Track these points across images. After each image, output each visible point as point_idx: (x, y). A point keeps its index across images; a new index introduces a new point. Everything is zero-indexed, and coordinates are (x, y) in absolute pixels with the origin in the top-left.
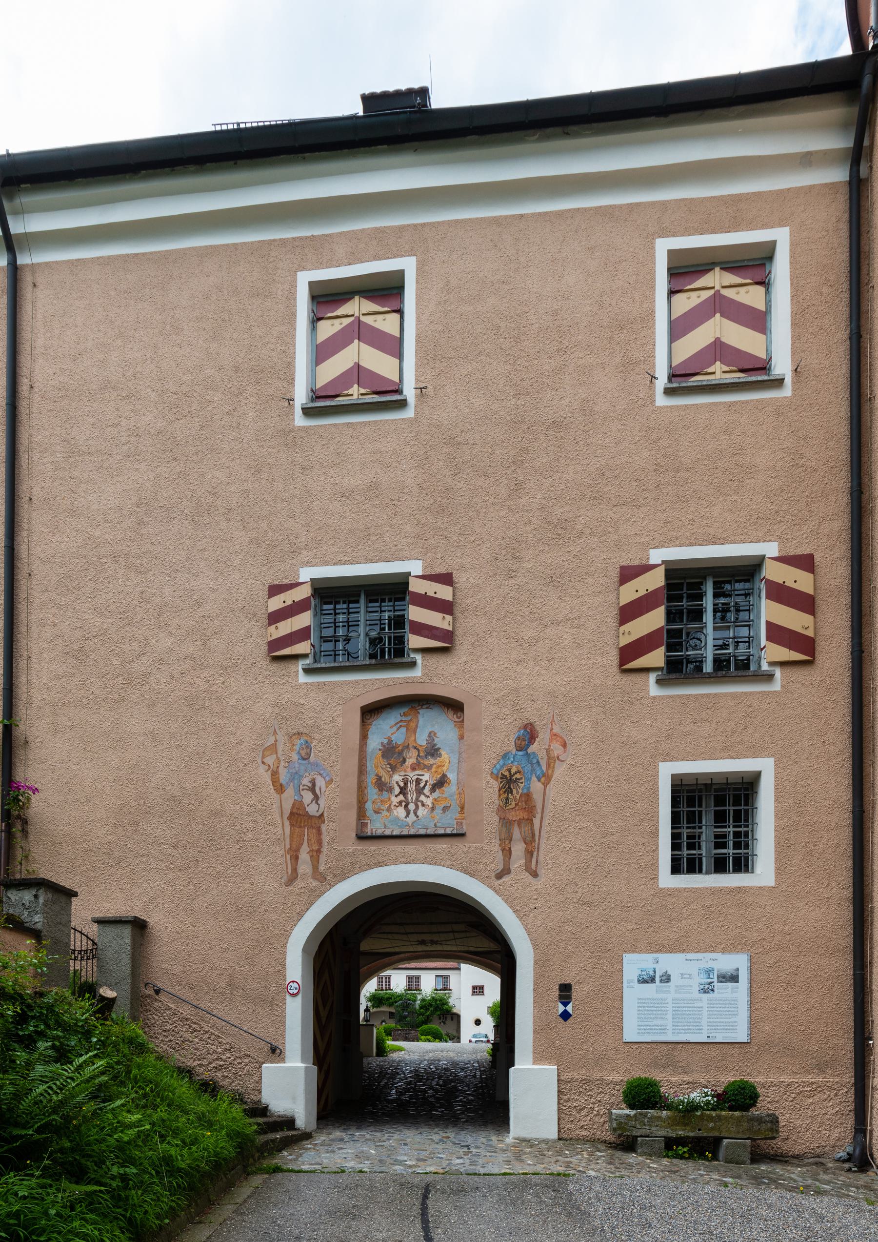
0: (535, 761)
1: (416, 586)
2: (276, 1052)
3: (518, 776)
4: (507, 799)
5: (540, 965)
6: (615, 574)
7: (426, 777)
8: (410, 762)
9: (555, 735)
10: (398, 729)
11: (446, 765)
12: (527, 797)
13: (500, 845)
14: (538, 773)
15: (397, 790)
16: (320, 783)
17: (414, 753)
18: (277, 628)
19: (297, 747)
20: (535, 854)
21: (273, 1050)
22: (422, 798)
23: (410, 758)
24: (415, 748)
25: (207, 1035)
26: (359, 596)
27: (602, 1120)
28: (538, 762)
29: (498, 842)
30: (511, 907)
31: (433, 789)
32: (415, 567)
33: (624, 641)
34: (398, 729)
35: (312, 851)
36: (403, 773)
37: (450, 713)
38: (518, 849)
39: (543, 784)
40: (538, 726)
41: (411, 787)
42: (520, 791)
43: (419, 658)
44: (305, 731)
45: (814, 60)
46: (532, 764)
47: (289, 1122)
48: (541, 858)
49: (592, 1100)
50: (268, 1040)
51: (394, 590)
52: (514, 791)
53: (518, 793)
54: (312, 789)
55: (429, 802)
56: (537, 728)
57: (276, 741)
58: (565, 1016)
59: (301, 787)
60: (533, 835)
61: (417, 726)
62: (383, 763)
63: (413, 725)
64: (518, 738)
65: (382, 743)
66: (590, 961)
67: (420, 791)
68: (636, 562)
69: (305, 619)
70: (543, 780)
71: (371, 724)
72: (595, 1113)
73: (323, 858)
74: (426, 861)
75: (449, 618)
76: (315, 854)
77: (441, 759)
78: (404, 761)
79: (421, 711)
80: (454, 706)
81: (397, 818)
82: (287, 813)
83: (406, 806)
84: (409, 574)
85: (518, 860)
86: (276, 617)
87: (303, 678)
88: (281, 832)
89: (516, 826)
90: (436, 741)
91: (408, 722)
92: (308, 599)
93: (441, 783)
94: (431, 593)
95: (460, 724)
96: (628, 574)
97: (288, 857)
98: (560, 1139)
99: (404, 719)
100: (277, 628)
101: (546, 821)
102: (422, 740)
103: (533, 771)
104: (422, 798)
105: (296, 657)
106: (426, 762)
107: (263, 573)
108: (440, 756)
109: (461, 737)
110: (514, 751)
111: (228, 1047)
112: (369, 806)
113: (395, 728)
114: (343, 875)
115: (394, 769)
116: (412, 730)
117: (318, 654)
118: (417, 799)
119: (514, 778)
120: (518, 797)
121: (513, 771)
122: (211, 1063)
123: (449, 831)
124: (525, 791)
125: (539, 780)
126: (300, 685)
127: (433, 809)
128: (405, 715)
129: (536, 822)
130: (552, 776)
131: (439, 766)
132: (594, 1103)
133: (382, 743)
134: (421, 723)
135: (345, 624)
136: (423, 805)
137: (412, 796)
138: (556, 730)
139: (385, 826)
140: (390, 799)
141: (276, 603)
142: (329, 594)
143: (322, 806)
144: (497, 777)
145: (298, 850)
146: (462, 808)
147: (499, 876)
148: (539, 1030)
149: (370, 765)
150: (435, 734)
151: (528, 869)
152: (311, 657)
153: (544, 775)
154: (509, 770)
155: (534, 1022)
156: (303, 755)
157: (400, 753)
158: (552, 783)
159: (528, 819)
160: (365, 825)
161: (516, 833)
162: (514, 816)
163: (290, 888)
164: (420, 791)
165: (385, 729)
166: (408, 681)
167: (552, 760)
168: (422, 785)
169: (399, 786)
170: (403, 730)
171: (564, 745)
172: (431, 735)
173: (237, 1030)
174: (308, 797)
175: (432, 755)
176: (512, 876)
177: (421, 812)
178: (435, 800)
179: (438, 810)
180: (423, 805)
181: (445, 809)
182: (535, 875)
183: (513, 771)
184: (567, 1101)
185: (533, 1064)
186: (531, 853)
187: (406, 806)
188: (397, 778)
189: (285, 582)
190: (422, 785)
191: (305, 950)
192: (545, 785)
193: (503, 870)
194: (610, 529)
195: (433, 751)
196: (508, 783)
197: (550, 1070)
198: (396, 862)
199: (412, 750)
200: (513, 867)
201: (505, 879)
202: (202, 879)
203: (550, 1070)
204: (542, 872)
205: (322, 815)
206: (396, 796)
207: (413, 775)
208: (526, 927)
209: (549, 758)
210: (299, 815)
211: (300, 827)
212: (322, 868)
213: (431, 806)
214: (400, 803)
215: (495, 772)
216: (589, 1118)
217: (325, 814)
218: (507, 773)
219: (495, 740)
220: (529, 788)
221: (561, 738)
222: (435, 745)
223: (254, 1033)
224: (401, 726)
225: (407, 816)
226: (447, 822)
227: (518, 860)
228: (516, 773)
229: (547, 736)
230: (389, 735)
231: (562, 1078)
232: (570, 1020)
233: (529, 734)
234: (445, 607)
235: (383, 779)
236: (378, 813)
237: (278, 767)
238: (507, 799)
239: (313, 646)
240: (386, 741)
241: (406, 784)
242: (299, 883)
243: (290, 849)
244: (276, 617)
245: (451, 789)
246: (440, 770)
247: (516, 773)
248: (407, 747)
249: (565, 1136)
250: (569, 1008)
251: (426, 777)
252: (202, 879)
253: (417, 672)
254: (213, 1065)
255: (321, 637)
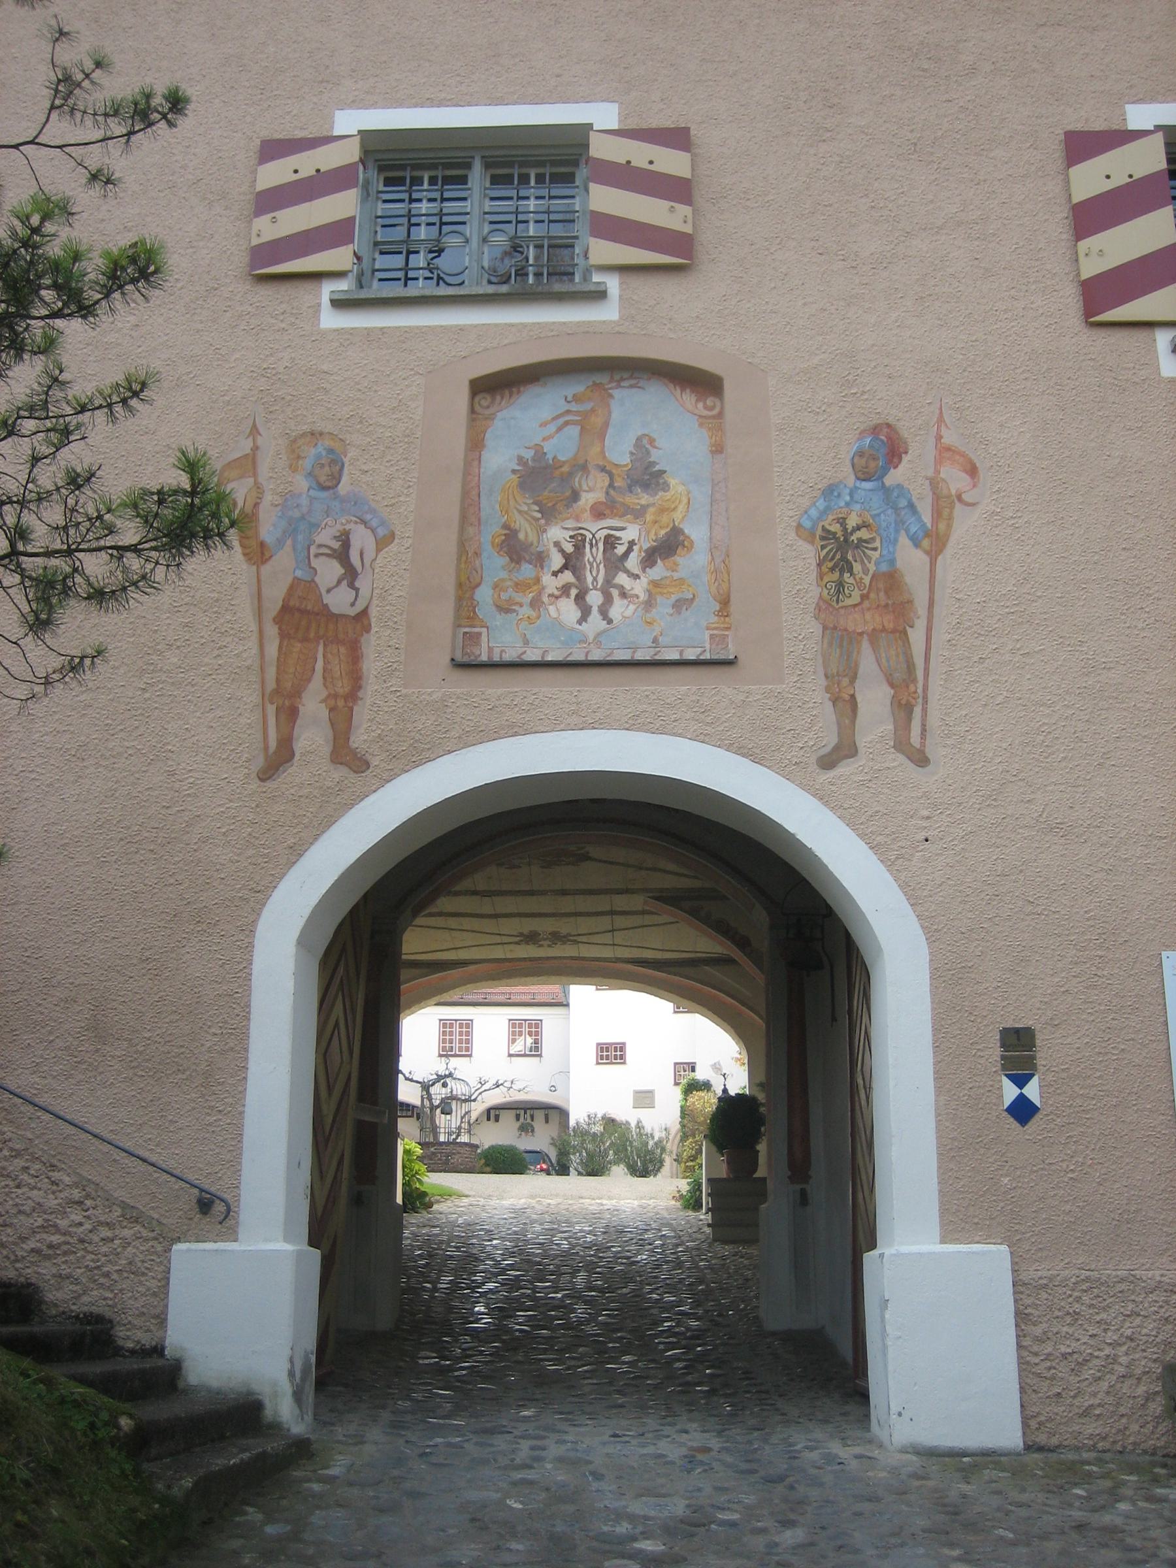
0: (903, 503)
1: (600, 148)
2: (212, 1209)
3: (864, 534)
4: (840, 585)
5: (949, 981)
6: (1055, 149)
7: (631, 532)
8: (588, 499)
9: (948, 449)
10: (560, 429)
11: (682, 508)
12: (891, 580)
13: (828, 689)
14: (913, 529)
15: (557, 561)
16: (362, 539)
17: (602, 481)
18: (274, 220)
19: (307, 464)
20: (918, 710)
21: (205, 1205)
22: (622, 579)
23: (591, 490)
24: (603, 469)
25: (20, 1163)
26: (468, 166)
27: (1141, 1390)
28: (911, 506)
29: (822, 682)
30: (862, 836)
31: (649, 560)
32: (602, 116)
33: (1091, 268)
34: (560, 429)
35: (335, 696)
36: (570, 524)
37: (689, 398)
38: (874, 698)
39: (927, 553)
40: (905, 430)
41: (593, 555)
42: (872, 568)
43: (613, 283)
44: (328, 427)
45: (792, 831)
46: (896, 510)
47: (243, 1414)
48: (934, 720)
49: (1111, 1337)
50: (191, 1177)
51: (552, 160)
52: (857, 567)
53: (866, 571)
54: (342, 554)
55: (639, 588)
56: (905, 434)
57: (255, 448)
58: (1023, 1111)
59: (313, 550)
60: (910, 667)
61: (606, 424)
62: (525, 503)
63: (596, 421)
64: (860, 453)
65: (520, 459)
66: (1077, 970)
67: (615, 564)
68: (1098, 126)
69: (343, 205)
70: (926, 543)
71: (491, 418)
72: (1121, 1370)
73: (363, 713)
74: (634, 724)
75: (684, 210)
76: (341, 703)
77: (668, 495)
78: (575, 496)
79: (616, 393)
80: (699, 382)
81: (558, 623)
82: (273, 605)
83: (580, 599)
84: (590, 126)
85: (312, 737)
86: (272, 200)
87: (331, 320)
88: (255, 650)
89: (865, 645)
90: (655, 455)
91: (586, 415)
92: (351, 167)
93: (669, 546)
94: (640, 162)
95: (715, 423)
96: (1082, 146)
97: (271, 710)
98: (1028, 1448)
99: (574, 407)
100: (274, 220)
101: (941, 635)
102: (619, 451)
103: (900, 523)
104: (622, 579)
105: (317, 276)
106: (630, 500)
107: (249, 119)
108: (666, 487)
109: (718, 449)
110: (851, 480)
111: (76, 1194)
112: (484, 594)
113: (552, 428)
114: (418, 753)
115: (549, 513)
116: (593, 430)
117: (368, 273)
118: (608, 582)
119: (854, 538)
120: (867, 580)
121: (852, 522)
122: (23, 1239)
123: (690, 655)
124: (884, 567)
125: (917, 544)
126: (324, 333)
127: (649, 604)
128: (577, 399)
129: (916, 636)
130: (947, 536)
131: (662, 510)
132: (1115, 1345)
133: (520, 459)
134: (616, 414)
135: (435, 219)
136: (623, 595)
137: (595, 574)
138: (949, 438)
139: (526, 642)
140: (538, 580)
141: (276, 173)
142: (403, 165)
143: (365, 591)
144: (813, 535)
145: (297, 693)
146: (725, 602)
147: (828, 762)
148: (953, 1150)
149: (490, 507)
150: (652, 441)
151: (901, 745)
152: (351, 278)
153: (927, 534)
154: (842, 522)
155: (938, 1130)
156: (323, 479)
157: (566, 478)
158: (949, 551)
159: (894, 631)
160: (473, 639)
161: (867, 662)
162: (855, 622)
163: (270, 785)
164: (615, 564)
165: (530, 425)
166: (587, 330)
167: (944, 504)
168: (620, 550)
169: (562, 551)
170: (574, 431)
171: (972, 471)
172: (643, 445)
173: (106, 1148)
174: (328, 571)
175: (646, 486)
176: (861, 760)
177: (618, 609)
178: (655, 584)
179: (663, 607)
180: (623, 595)
181: (680, 605)
182: (921, 759)
183: (852, 522)
184: (1039, 1340)
185: (943, 1242)
186: (908, 709)
187: (580, 599)
188: (558, 533)
189: (299, 134)
190: (620, 550)
191: (303, 941)
192: (934, 555)
193: (836, 748)
194: (1035, 65)
195: (648, 477)
196: (839, 550)
197: (991, 1261)
198: (556, 724)
199: (594, 472)
200: (863, 741)
201: (845, 769)
202: (38, 761)
203: (991, 1261)
204: (935, 751)
205: (365, 613)
206: (555, 574)
207: (597, 529)
208: (904, 886)
209: (937, 497)
210: (303, 612)
211: (305, 639)
212: (359, 739)
213: (643, 597)
214: (565, 590)
215: (807, 524)
216: (1104, 1385)
217: (374, 612)
218: (835, 528)
219: (806, 461)
220: (892, 562)
221: (963, 455)
222: (654, 464)
223: (153, 1158)
224: (567, 423)
225: (583, 619)
226: (691, 635)
227: (312, 737)
228: (858, 528)
229: (931, 453)
230: (538, 440)
231: (1024, 1277)
232: (1035, 1123)
233: (884, 449)
234: (677, 190)
235: (521, 536)
236: (508, 611)
237: (256, 505)
238: (840, 585)
239: (359, 258)
240: (528, 455)
241: (579, 546)
242: (294, 774)
243: (277, 691)
244: (272, 200)
245: (694, 563)
246: (665, 519)
247: (858, 528)
248: (584, 468)
249: (1042, 1439)
250: (1032, 1091)
251: (631, 532)
252: (38, 761)
253: (607, 313)
254: (32, 1244)
255: (376, 244)
